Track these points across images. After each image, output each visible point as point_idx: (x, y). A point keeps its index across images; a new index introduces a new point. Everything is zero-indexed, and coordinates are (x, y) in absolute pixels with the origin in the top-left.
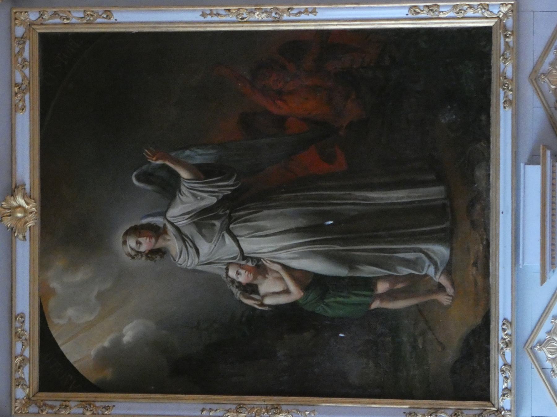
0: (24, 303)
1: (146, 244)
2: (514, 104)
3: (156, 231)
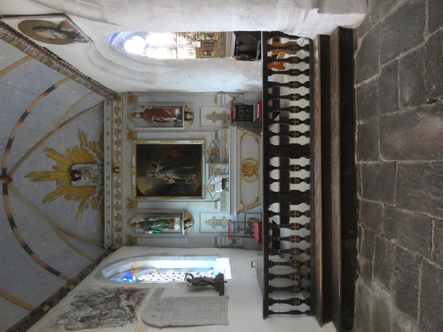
0: (134, 184)
1: (152, 175)
2: (205, 155)
3: (154, 173)
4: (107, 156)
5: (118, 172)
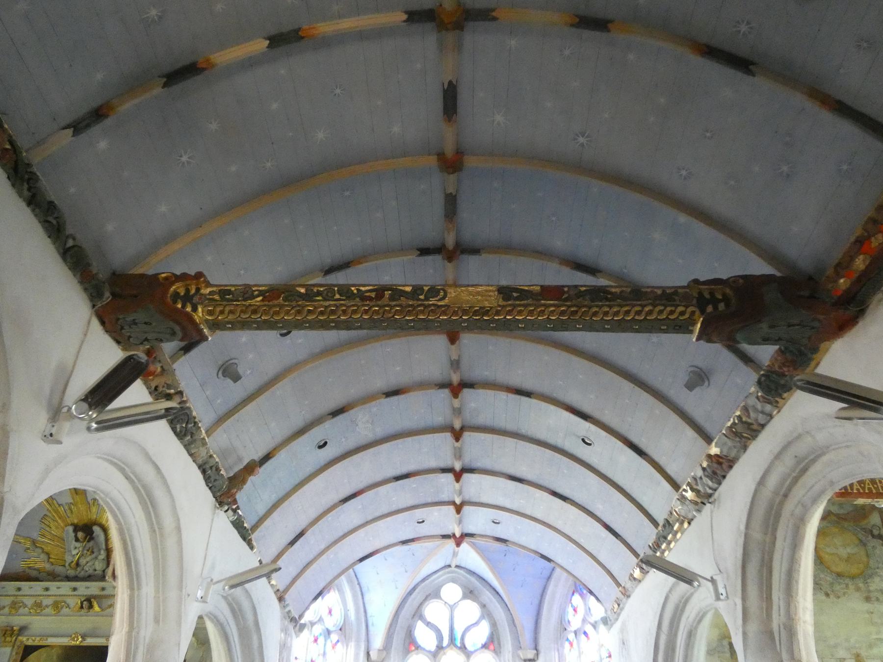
0: (51, 641)
4: (87, 588)
5: (82, 607)
